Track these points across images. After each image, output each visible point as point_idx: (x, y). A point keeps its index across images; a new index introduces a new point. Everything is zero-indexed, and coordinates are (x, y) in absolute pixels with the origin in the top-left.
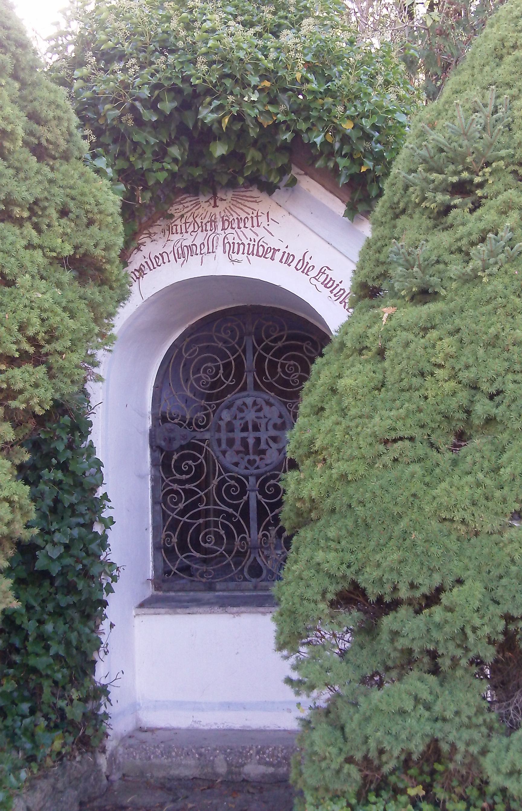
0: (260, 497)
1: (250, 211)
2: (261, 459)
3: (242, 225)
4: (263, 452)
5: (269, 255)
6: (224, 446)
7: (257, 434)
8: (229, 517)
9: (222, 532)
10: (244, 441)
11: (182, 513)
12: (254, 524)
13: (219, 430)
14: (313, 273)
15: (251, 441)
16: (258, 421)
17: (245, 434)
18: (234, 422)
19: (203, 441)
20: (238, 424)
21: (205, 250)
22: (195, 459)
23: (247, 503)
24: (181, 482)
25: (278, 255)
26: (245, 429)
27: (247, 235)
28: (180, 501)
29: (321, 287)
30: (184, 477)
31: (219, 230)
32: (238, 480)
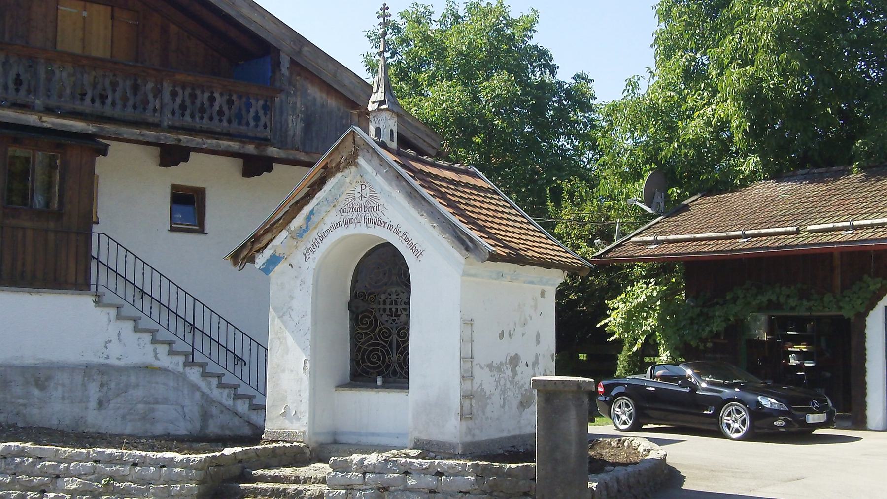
4: (399, 315)
8: (384, 347)
10: (391, 309)
14: (401, 235)
15: (394, 310)
20: (388, 301)
24: (363, 329)
25: (387, 225)
26: (391, 304)
27: (310, 332)
32: (388, 329)
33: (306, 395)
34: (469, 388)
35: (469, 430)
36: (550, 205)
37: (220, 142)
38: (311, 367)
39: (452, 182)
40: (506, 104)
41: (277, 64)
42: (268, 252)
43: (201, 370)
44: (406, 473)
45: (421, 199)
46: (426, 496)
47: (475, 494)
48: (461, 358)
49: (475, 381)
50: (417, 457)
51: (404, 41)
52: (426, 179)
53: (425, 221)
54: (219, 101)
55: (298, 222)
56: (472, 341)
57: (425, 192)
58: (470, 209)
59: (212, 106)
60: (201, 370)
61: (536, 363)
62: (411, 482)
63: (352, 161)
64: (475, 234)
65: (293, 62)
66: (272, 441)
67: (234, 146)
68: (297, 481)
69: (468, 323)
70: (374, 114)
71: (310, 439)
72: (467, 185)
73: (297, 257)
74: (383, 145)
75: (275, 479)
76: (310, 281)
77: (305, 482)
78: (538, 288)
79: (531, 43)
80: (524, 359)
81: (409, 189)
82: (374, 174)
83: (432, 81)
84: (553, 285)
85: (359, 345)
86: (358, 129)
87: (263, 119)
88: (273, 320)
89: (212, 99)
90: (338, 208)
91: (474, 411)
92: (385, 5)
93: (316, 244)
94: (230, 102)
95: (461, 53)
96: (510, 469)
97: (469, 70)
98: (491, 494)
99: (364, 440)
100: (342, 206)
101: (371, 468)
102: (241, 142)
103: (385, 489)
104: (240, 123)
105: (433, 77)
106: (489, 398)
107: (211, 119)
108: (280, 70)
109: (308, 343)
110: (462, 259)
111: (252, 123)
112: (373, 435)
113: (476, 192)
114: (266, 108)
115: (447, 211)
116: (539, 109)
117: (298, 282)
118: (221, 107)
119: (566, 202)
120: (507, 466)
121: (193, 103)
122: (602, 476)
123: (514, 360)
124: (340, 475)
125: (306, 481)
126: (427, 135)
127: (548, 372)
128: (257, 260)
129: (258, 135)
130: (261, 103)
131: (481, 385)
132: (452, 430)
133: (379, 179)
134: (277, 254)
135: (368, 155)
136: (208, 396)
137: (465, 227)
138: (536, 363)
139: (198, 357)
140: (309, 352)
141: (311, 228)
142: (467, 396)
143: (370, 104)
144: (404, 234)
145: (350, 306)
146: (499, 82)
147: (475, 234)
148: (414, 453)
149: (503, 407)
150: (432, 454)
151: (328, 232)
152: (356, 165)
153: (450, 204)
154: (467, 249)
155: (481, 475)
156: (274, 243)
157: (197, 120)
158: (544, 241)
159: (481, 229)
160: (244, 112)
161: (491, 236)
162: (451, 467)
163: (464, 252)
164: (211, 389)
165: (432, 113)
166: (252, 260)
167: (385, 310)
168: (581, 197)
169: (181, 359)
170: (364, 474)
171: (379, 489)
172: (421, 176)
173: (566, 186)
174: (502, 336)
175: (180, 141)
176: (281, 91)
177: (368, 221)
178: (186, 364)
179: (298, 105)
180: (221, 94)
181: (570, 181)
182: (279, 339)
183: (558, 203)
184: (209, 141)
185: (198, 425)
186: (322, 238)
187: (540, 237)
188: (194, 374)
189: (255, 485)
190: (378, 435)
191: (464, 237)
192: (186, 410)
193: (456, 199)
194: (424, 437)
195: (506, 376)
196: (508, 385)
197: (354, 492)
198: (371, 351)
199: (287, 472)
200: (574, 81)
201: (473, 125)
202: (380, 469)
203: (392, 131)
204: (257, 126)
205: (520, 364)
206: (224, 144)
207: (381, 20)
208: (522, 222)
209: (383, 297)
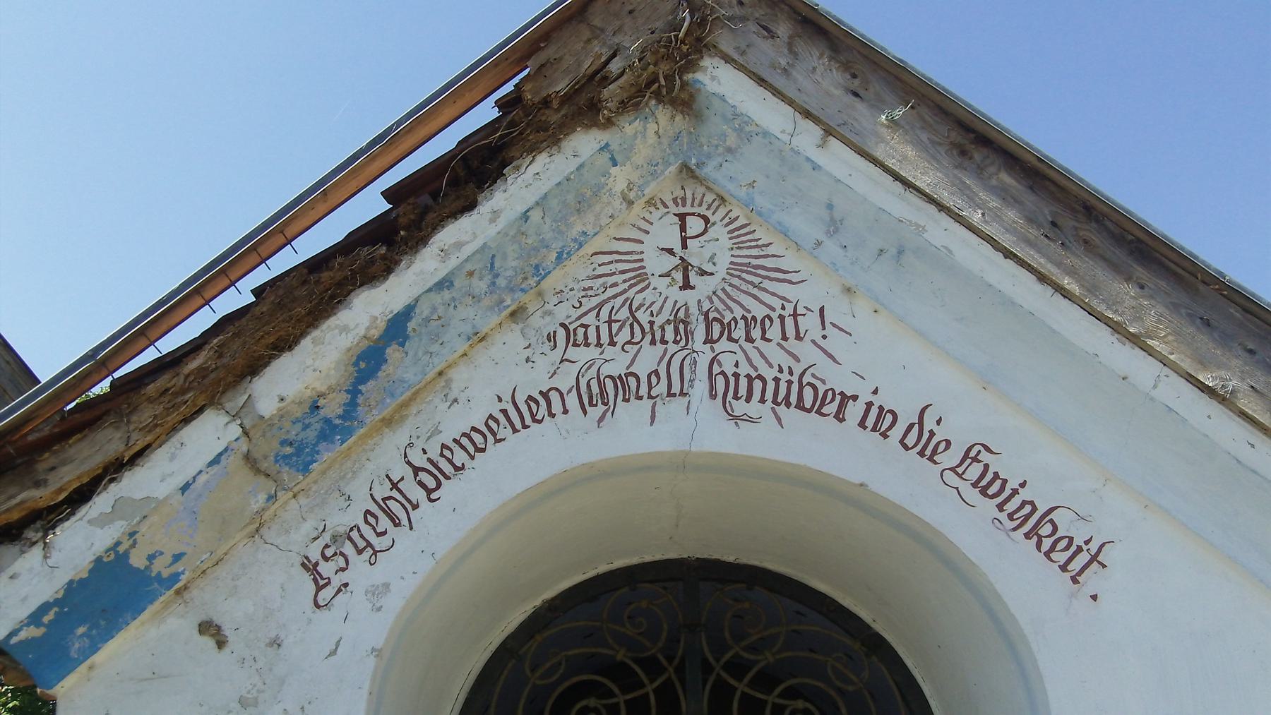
1: (777, 303)
5: (831, 408)
14: (949, 459)
21: (662, 388)
25: (854, 411)
29: (973, 495)
42: (79, 543)
90: (540, 323)
93: (391, 510)
100: (564, 312)
134: (137, 560)
135: (766, 52)
144: (969, 456)
151: (476, 441)
152: (685, 101)
156: (134, 484)
177: (730, 391)
186: (433, 477)
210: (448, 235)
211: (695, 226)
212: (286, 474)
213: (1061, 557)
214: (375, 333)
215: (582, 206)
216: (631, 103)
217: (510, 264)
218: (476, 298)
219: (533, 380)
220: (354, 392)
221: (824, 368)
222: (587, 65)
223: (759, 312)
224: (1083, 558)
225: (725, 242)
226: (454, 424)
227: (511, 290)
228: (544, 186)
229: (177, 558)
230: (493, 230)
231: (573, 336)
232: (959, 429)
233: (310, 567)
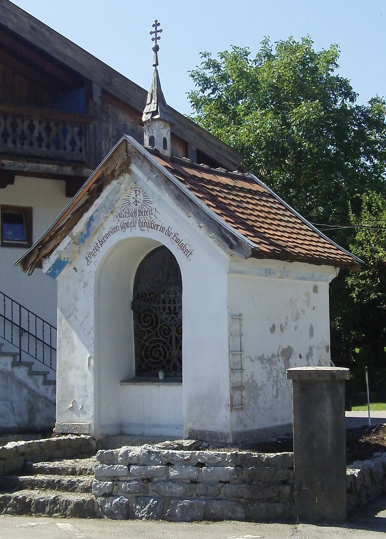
0: (176, 334)
1: (149, 207)
2: (177, 317)
3: (146, 214)
5: (155, 228)
6: (162, 310)
7: (175, 305)
8: (164, 343)
9: (162, 350)
10: (169, 308)
11: (146, 341)
12: (174, 347)
13: (159, 303)
14: (172, 236)
15: (172, 308)
16: (175, 299)
17: (169, 305)
18: (165, 299)
19: (154, 308)
20: (167, 300)
21: (132, 225)
22: (150, 316)
23: (171, 337)
25: (159, 227)
26: (170, 302)
28: (144, 336)
29: (174, 242)
30: (146, 324)
31: (137, 216)
33: (91, 390)
34: (239, 379)
35: (240, 420)
36: (352, 217)
37: (41, 165)
38: (94, 365)
39: (226, 186)
40: (312, 128)
41: (90, 94)
42: (53, 258)
43: (27, 369)
44: (169, 464)
45: (187, 201)
46: (188, 486)
47: (234, 484)
48: (230, 351)
49: (245, 373)
50: (189, 448)
51: (224, 78)
52: (196, 184)
53: (192, 221)
54: (38, 128)
55: (79, 228)
56: (241, 335)
57: (192, 195)
58: (240, 210)
59: (31, 132)
60: (27, 369)
61: (310, 355)
62: (173, 473)
63: (125, 169)
64: (239, 233)
65: (104, 92)
66: (62, 434)
67: (53, 168)
68: (74, 472)
69: (236, 318)
70: (148, 124)
71: (95, 431)
72: (242, 189)
73: (80, 262)
74: (156, 153)
75: (54, 471)
76: (92, 283)
77: (81, 474)
78: (311, 284)
79: (332, 74)
80: (296, 351)
81: (177, 192)
82: (146, 180)
83: (248, 110)
84: (325, 281)
85: (142, 342)
86: (130, 138)
87: (79, 144)
88: (61, 320)
89: (32, 127)
90: (116, 214)
91: (246, 402)
92: (156, 21)
93: (96, 249)
94: (48, 129)
95: (271, 85)
96: (268, 458)
97: (279, 99)
98: (250, 483)
99: (147, 431)
100: (119, 211)
101: (135, 460)
102: (59, 164)
103: (149, 480)
104: (57, 148)
105: (248, 108)
106: (261, 389)
107: (31, 144)
108: (93, 99)
109: (91, 341)
110: (227, 257)
111: (69, 148)
112: (155, 426)
113: (250, 196)
114: (81, 134)
115: (212, 212)
116: (340, 132)
117: (82, 285)
118: (40, 134)
119: (365, 214)
120: (266, 455)
121: (14, 131)
122: (367, 462)
123: (287, 353)
124: (107, 467)
125: (83, 472)
126: (229, 154)
127: (323, 363)
128: (44, 265)
129: (75, 158)
130: (76, 129)
131: (252, 376)
132: (222, 420)
133: (150, 184)
134: (62, 259)
135: (139, 162)
136: (34, 392)
137: (229, 227)
138: (310, 355)
139: (25, 358)
140: (92, 349)
141: (92, 233)
142: (236, 388)
143: (144, 115)
145: (134, 306)
146: (306, 109)
147: (239, 233)
148: (187, 443)
149: (276, 397)
150: (205, 444)
151: (107, 236)
152: (129, 172)
153: (219, 206)
154: (231, 247)
155: (240, 463)
157: (19, 145)
158: (316, 239)
159: (249, 228)
160: (61, 138)
161: (257, 234)
162: (211, 458)
163: (229, 250)
164: (38, 386)
165: (247, 139)
166: (40, 265)
167: (164, 309)
168: (378, 207)
169: (9, 360)
170: (129, 466)
171: (143, 480)
172: (192, 181)
173: (366, 198)
174: (273, 329)
175: (3, 165)
176: (95, 117)
177: (142, 225)
178: (14, 364)
179: (110, 130)
180: (40, 122)
181: (368, 194)
182: (66, 338)
183: (357, 211)
184: (30, 165)
185: (26, 418)
186: (102, 242)
187: (312, 236)
188: (21, 373)
189: (32, 477)
190: (160, 426)
191: (228, 236)
192: (15, 405)
193: (227, 202)
194: (198, 427)
195: (278, 368)
196: (281, 376)
197: (120, 483)
198: (153, 348)
199: (68, 463)
200: (370, 105)
201: (283, 148)
202: (144, 461)
203: (165, 140)
204: (73, 150)
205: (293, 356)
206: (44, 167)
207: (154, 35)
208: (295, 223)
209: (162, 296)
210: (96, 202)
211: (138, 192)
212: (81, 244)
213: (186, 253)
214: (88, 220)
215: (117, 193)
216: (120, 175)
217: (108, 205)
218: (103, 211)
219: (114, 225)
220: (88, 230)
221: (155, 220)
222: (113, 168)
223: (146, 209)
224: (189, 253)
225: (142, 196)
226: (105, 232)
227: (110, 208)
228: (109, 192)
229: (68, 258)
230: (103, 200)
231: (120, 216)
232: (173, 231)
233: (87, 258)
